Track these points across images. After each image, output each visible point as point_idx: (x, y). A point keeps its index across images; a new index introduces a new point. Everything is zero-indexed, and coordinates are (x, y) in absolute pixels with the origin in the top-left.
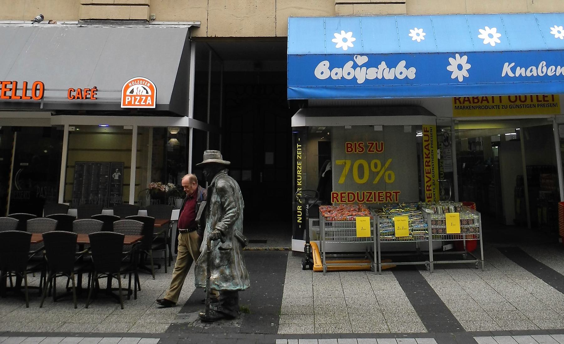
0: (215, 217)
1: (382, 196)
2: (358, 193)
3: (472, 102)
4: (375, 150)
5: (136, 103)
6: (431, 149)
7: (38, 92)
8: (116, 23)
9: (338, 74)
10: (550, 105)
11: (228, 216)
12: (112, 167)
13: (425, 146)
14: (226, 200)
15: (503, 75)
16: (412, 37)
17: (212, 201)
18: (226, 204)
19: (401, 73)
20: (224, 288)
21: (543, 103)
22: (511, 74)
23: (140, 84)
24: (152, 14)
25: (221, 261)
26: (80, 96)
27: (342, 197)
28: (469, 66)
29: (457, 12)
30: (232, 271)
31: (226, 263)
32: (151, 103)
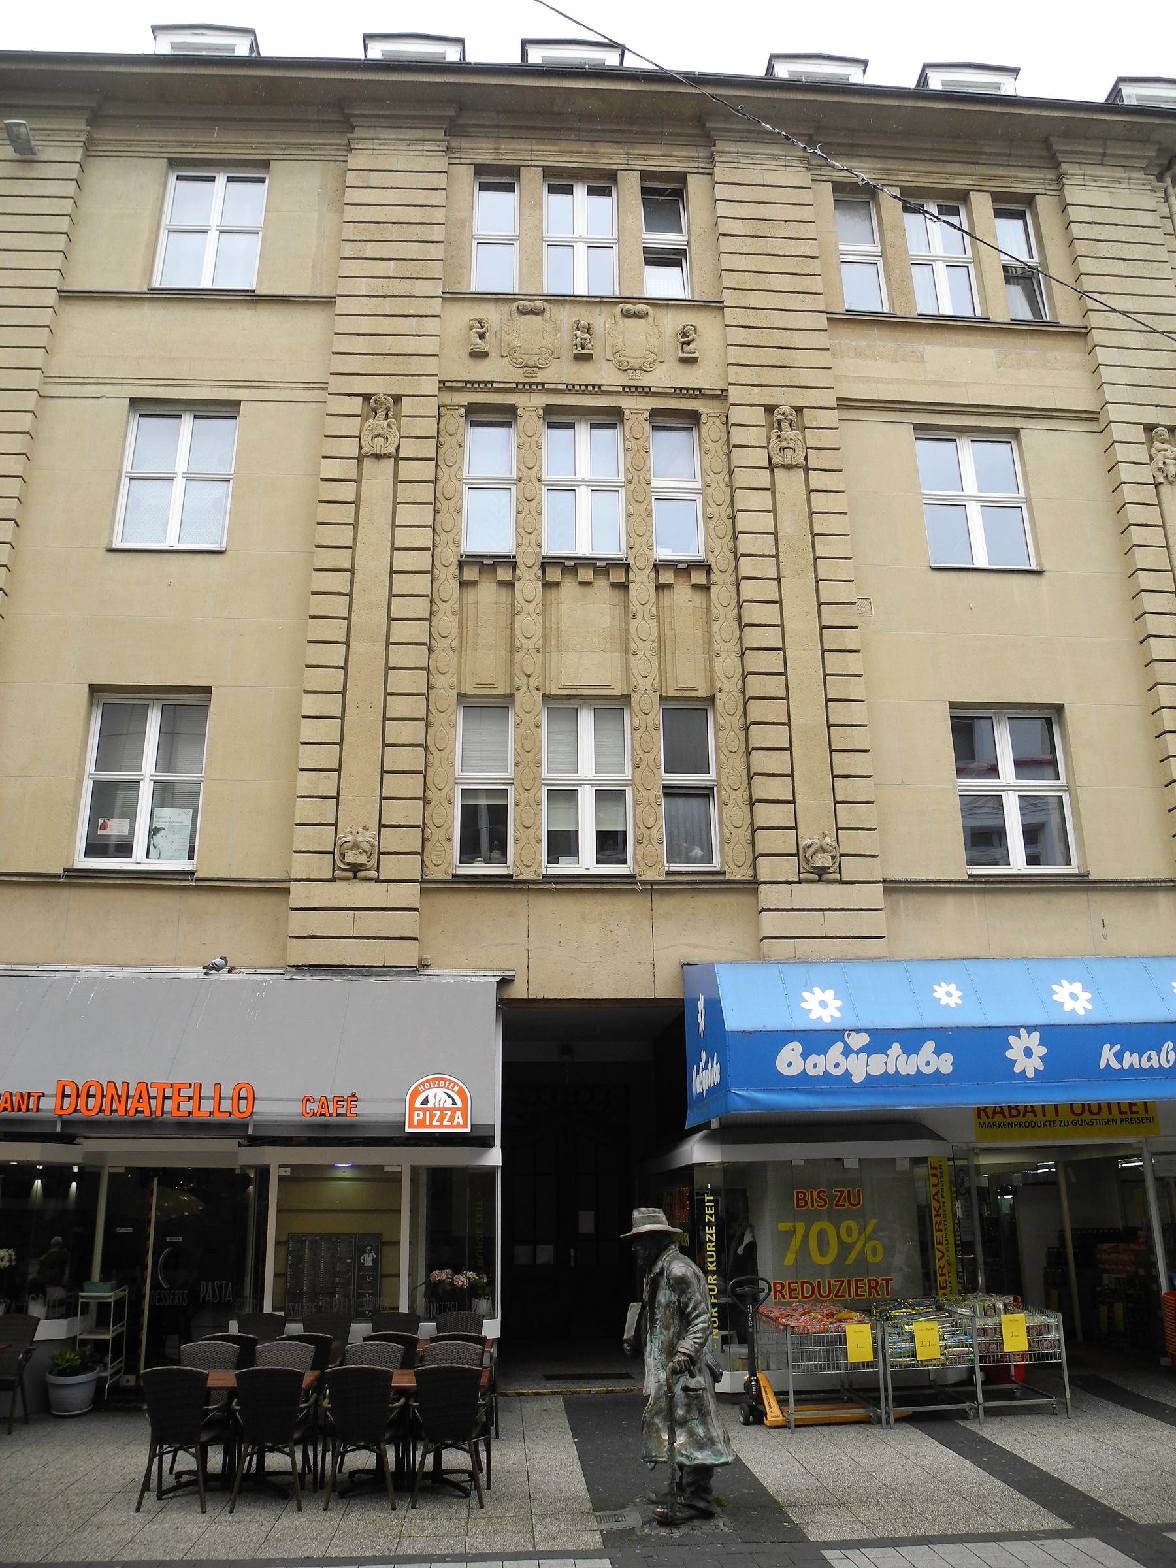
0: (669, 1330)
1: (862, 1288)
2: (819, 1282)
3: (1007, 1114)
4: (847, 1204)
5: (434, 1123)
6: (941, 1199)
7: (67, 1100)
8: (359, 972)
9: (817, 1065)
10: (1141, 1121)
11: (696, 1328)
12: (361, 1243)
13: (934, 1195)
14: (690, 1299)
15: (1102, 1065)
16: (1088, 1001)
17: (659, 1301)
18: (691, 1306)
19: (928, 1064)
20: (700, 1462)
21: (1129, 1116)
22: (1115, 1065)
23: (439, 1087)
24: (425, 956)
25: (688, 1411)
26: (8, 1106)
27: (790, 1290)
28: (1043, 1051)
29: (974, 954)
30: (708, 1430)
31: (696, 1414)
32: (461, 1123)
